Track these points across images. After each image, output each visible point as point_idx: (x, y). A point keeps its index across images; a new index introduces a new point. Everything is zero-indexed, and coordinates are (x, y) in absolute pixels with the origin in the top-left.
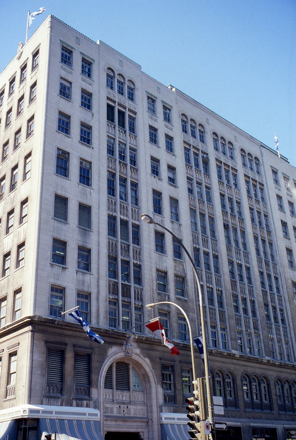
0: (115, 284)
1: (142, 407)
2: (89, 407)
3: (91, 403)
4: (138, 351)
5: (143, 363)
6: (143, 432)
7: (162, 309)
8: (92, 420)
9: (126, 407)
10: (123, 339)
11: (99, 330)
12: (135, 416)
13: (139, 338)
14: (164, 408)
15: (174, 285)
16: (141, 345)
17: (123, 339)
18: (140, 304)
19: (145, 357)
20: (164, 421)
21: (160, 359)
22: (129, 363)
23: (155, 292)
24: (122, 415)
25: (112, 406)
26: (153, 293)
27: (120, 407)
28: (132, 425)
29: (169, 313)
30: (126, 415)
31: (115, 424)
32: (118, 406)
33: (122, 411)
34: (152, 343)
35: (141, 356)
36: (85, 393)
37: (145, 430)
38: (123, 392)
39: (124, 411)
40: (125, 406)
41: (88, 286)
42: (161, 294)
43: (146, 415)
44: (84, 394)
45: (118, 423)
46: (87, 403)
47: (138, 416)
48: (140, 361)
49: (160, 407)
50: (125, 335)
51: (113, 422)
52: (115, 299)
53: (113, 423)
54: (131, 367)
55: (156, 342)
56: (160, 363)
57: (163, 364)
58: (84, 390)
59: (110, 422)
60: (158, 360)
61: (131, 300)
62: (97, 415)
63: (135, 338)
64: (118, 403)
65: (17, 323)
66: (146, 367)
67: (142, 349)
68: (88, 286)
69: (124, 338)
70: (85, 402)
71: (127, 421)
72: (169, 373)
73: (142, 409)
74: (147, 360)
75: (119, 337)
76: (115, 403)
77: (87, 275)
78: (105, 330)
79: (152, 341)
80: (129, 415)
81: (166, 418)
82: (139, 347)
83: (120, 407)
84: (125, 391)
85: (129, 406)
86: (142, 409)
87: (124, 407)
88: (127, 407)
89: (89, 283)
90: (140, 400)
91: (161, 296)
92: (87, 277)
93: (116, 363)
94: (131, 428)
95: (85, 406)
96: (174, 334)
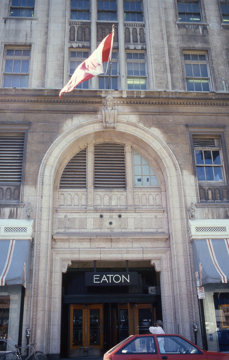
0: (85, 26)
1: (156, 214)
2: (16, 218)
3: (21, 211)
4: (133, 118)
5: (146, 138)
6: (159, 259)
7: (189, 47)
8: (12, 238)
9: (117, 217)
10: (96, 103)
11: (40, 93)
12: (138, 230)
13: (129, 95)
14: (198, 212)
15: (217, 9)
16: (141, 108)
17: (96, 103)
18: (139, 47)
19: (150, 127)
20: (195, 234)
21: (187, 126)
22: (124, 143)
23: (172, 25)
24: (107, 231)
25: (84, 217)
26: (167, 26)
27: (101, 216)
28: (130, 246)
29: (207, 50)
30: (116, 231)
31: (89, 246)
32: (98, 215)
33: (107, 224)
34: (163, 101)
35: (141, 125)
36: (11, 196)
37: (164, 256)
38: (112, 192)
39: (111, 223)
40: (115, 215)
41: (27, 35)
42: (187, 26)
43: (166, 227)
44: (9, 197)
45: (96, 244)
46: (11, 211)
47: (144, 230)
48: (138, 133)
49: (188, 210)
50: (98, 94)
51: (85, 243)
52: (83, 47)
53: (86, 245)
54: (128, 149)
55: (172, 98)
56: (188, 133)
57: (193, 135)
58: (9, 190)
59: (77, 243)
60: (183, 128)
61: (118, 44)
62: (24, 229)
63: (121, 98)
64: (96, 210)
65: (197, 190)
66: (153, 143)
67: (142, 114)
68: (27, 35)
69: (98, 100)
70: (7, 211)
71: (118, 240)
72: (214, 149)
73: (156, 217)
74: (156, 131)
75: (85, 100)
76: (89, 210)
77: (25, 21)
78: (52, 90)
79: (163, 98)
80: (123, 230)
81: (198, 229)
82: (136, 111)
83: (101, 216)
84: (115, 190)
85: (122, 214)
86: (156, 217)
87: (111, 217)
88: (120, 216)
89: (29, 32)
90: (151, 202)
91: (187, 29)
92: (25, 25)
93: (95, 147)
94: (128, 252)
95: (7, 217)
96: (221, 83)
